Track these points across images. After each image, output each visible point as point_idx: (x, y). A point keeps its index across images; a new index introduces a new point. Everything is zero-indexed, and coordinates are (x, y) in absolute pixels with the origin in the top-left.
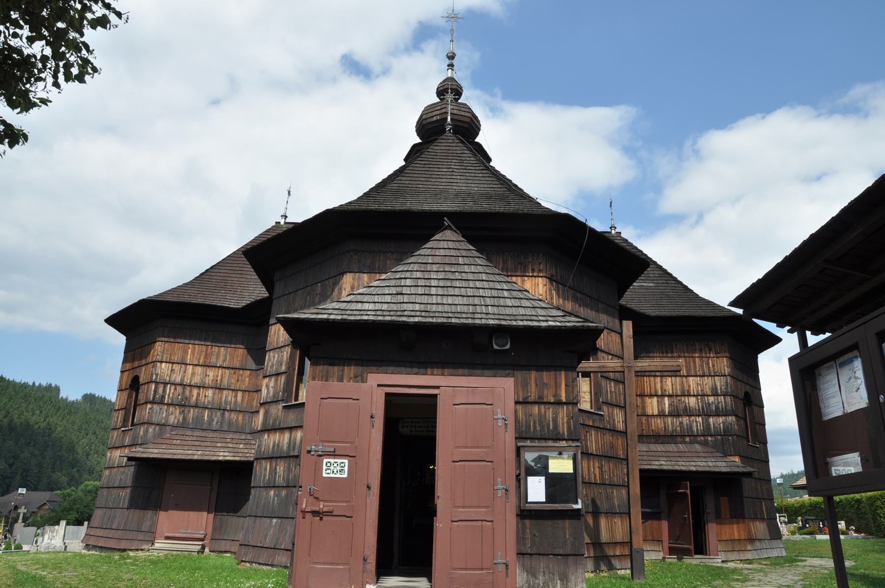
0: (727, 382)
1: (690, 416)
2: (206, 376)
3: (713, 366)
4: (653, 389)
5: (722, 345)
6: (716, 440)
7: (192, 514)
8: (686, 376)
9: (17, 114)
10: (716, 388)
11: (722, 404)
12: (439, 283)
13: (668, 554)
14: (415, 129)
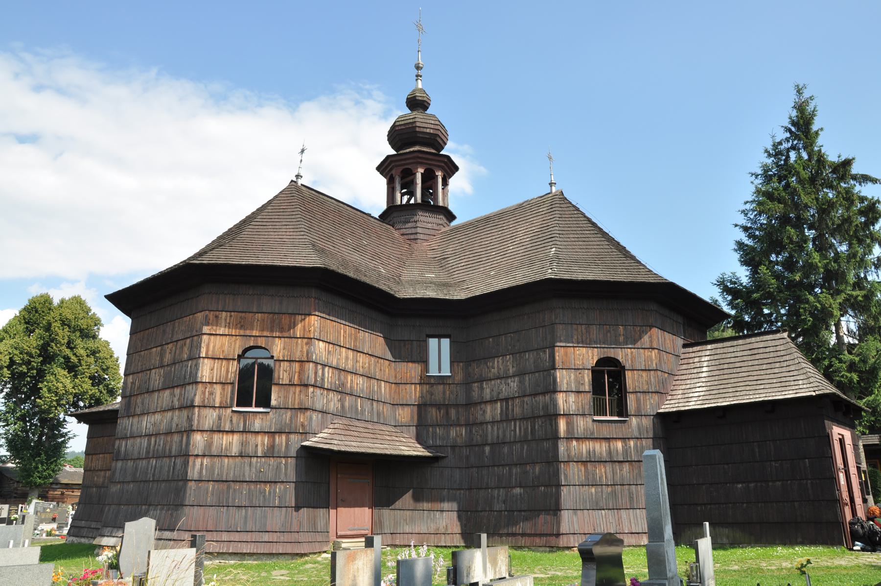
2: (357, 361)
7: (357, 510)
9: (874, 181)
12: (286, 397)
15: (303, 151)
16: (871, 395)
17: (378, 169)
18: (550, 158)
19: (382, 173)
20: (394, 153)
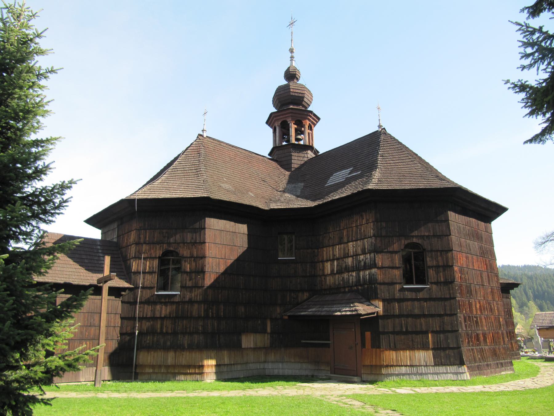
1: (349, 272)
10: (365, 249)
11: (368, 260)
13: (144, 257)
14: (272, 105)
17: (267, 123)
19: (269, 125)
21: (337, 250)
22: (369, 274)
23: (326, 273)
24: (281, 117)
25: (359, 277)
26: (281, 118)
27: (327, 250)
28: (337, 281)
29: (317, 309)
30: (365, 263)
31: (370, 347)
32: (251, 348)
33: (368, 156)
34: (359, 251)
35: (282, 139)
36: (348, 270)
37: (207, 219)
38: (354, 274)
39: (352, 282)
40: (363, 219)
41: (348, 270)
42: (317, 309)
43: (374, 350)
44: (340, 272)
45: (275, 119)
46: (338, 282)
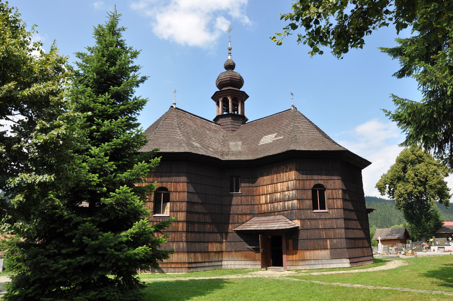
0: (293, 183)
1: (278, 202)
3: (288, 176)
4: (263, 192)
5: (293, 164)
6: (288, 212)
8: (276, 183)
10: (289, 187)
15: (175, 92)
16: (100, 297)
17: (212, 98)
18: (292, 94)
19: (214, 100)
20: (219, 90)
21: (270, 188)
22: (292, 204)
23: (261, 203)
24: (223, 95)
25: (285, 206)
26: (223, 96)
27: (262, 188)
28: (269, 208)
29: (257, 226)
30: (289, 196)
31: (292, 249)
32: (214, 252)
33: (287, 126)
34: (285, 189)
35: (223, 110)
36: (277, 201)
37: (365, 196)
38: (281, 203)
39: (280, 208)
40: (287, 168)
41: (277, 201)
42: (257, 226)
43: (294, 251)
44: (271, 202)
45: (219, 96)
46: (271, 208)
